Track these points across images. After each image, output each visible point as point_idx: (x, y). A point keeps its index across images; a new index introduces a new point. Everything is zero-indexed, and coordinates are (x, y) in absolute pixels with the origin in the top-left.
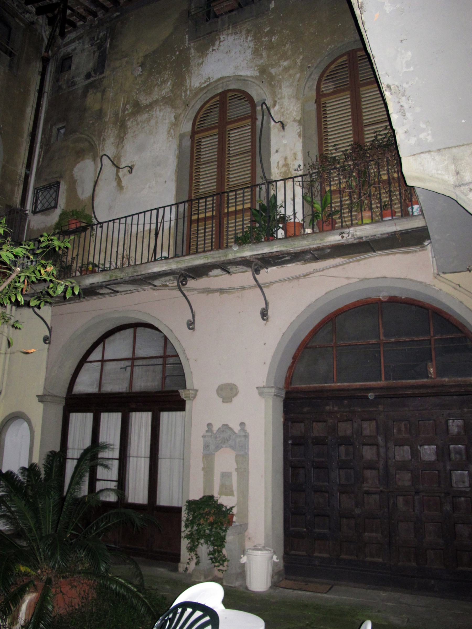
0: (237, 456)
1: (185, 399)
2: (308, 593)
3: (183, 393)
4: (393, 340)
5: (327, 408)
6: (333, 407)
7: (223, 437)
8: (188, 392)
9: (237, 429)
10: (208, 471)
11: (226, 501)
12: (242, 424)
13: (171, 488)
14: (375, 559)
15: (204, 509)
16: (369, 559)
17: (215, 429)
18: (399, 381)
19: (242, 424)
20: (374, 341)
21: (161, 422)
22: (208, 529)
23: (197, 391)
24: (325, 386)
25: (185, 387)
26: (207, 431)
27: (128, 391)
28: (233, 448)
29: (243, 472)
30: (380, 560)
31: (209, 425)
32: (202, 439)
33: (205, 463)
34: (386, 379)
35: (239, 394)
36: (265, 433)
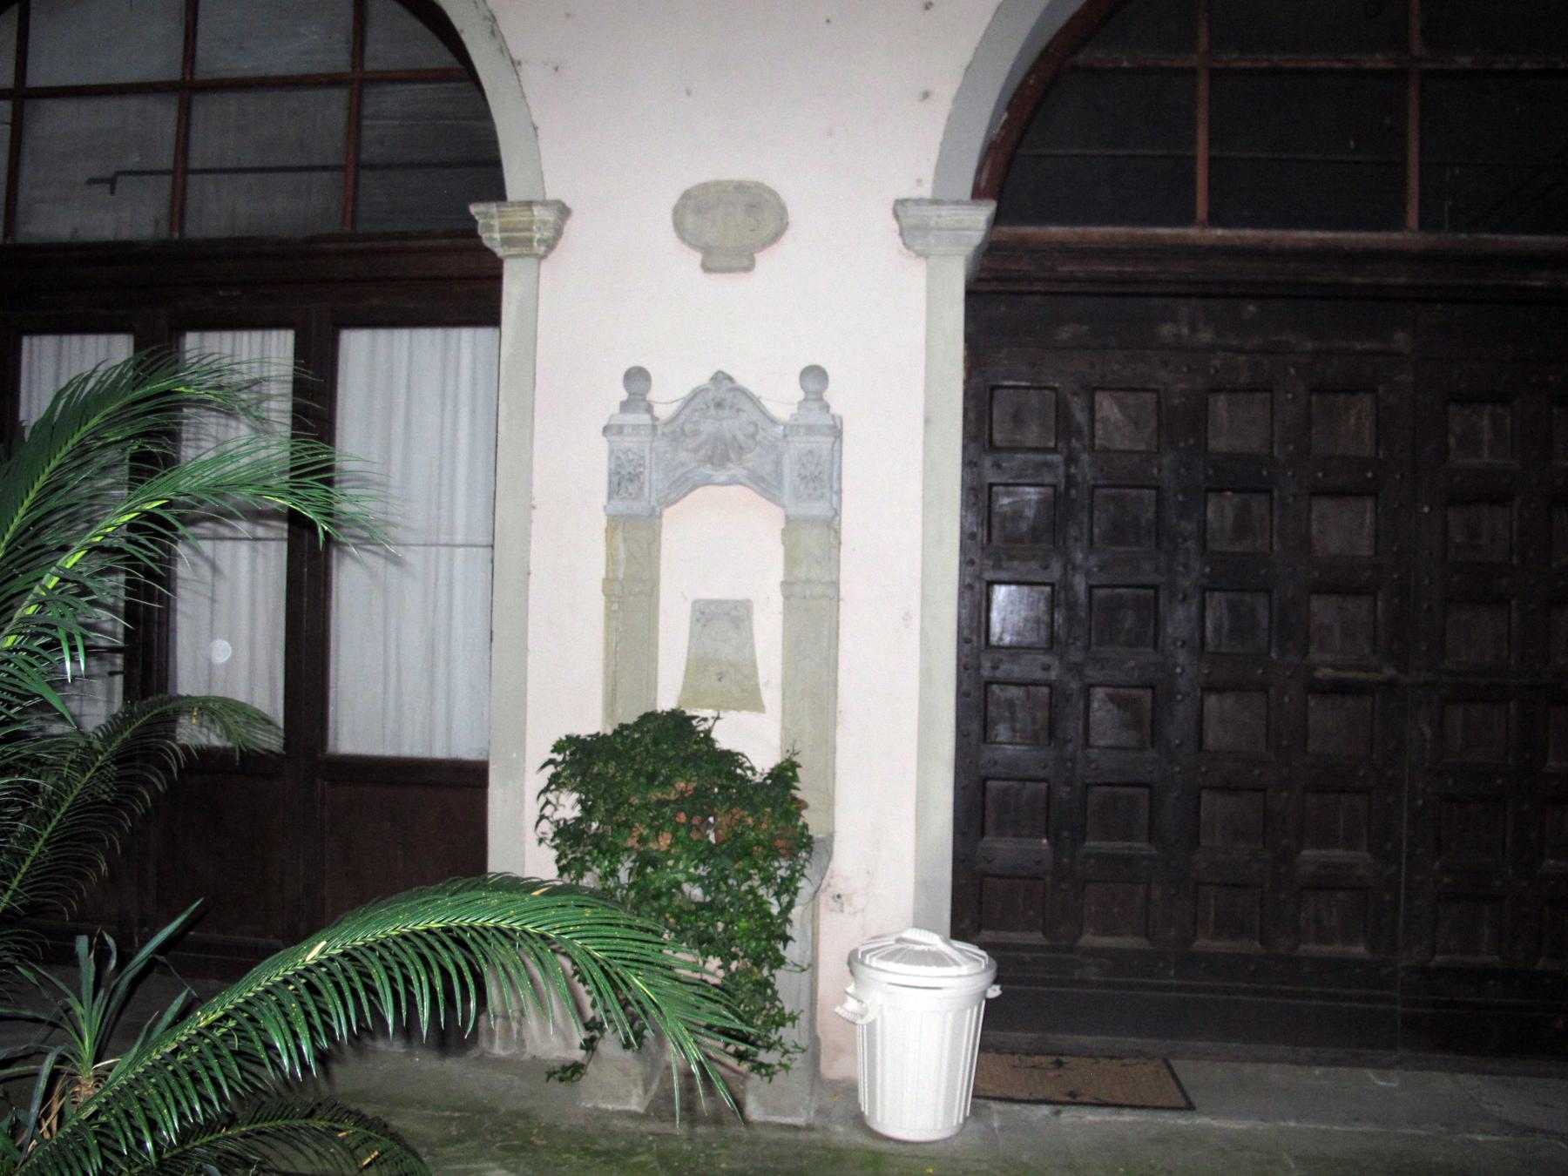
0: (792, 526)
1: (500, 252)
2: (1127, 1117)
3: (496, 223)
4: (1464, 61)
5: (1166, 330)
6: (1194, 329)
7: (712, 437)
8: (519, 217)
9: (782, 398)
10: (631, 595)
11: (753, 739)
12: (814, 376)
13: (393, 678)
14: (1335, 949)
15: (668, 782)
16: (1310, 948)
17: (667, 395)
18: (1486, 236)
19: (814, 376)
20: (1380, 61)
21: (340, 379)
22: (693, 880)
23: (564, 212)
24: (1158, 236)
25: (495, 191)
26: (625, 407)
27: (164, 233)
28: (767, 486)
29: (813, 598)
30: (1360, 950)
31: (637, 378)
32: (603, 445)
33: (622, 555)
34: (1423, 225)
35: (789, 233)
36: (927, 421)
